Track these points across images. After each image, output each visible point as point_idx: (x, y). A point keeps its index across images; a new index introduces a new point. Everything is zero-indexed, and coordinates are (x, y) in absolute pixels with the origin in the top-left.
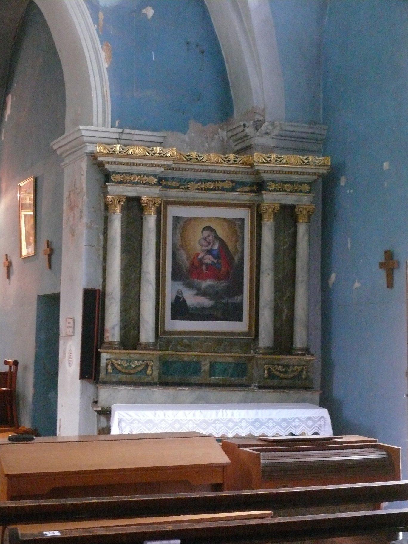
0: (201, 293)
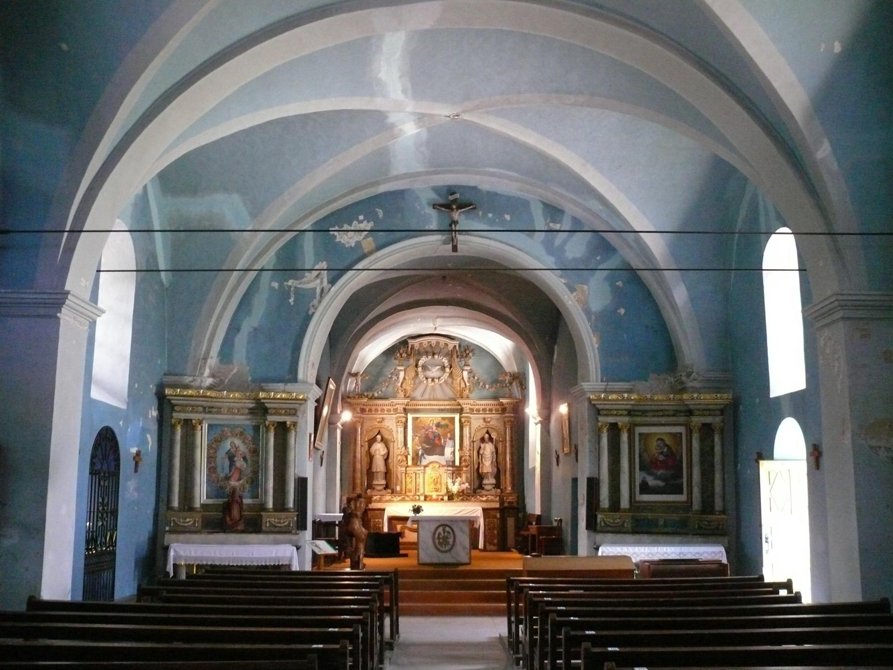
0: (657, 478)
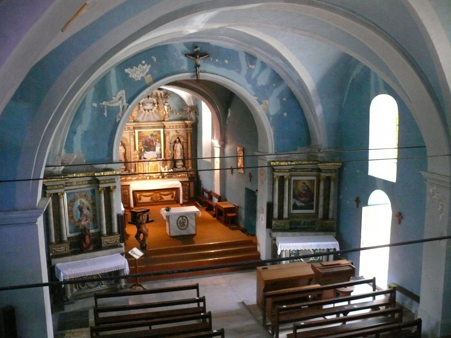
0: (301, 202)
